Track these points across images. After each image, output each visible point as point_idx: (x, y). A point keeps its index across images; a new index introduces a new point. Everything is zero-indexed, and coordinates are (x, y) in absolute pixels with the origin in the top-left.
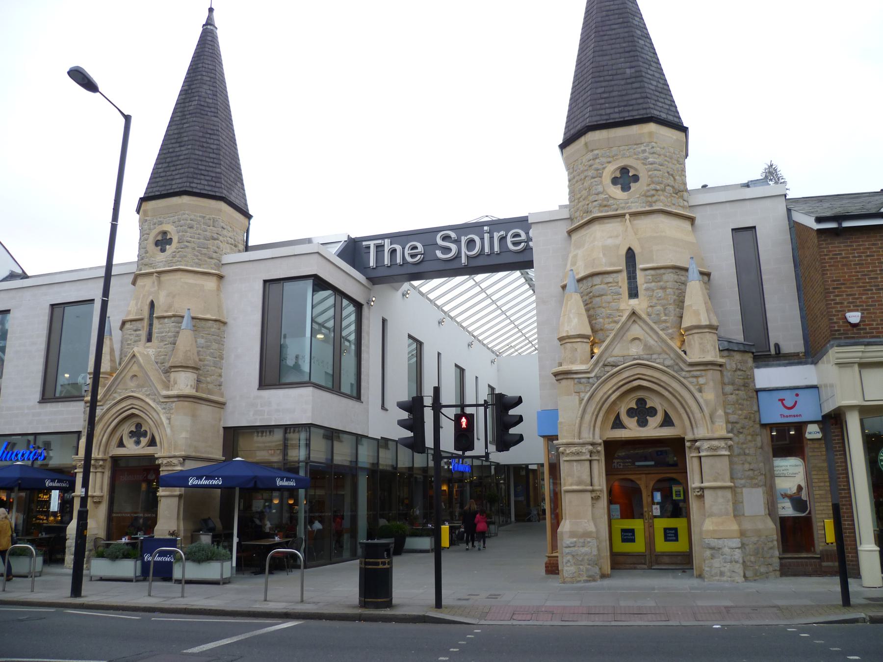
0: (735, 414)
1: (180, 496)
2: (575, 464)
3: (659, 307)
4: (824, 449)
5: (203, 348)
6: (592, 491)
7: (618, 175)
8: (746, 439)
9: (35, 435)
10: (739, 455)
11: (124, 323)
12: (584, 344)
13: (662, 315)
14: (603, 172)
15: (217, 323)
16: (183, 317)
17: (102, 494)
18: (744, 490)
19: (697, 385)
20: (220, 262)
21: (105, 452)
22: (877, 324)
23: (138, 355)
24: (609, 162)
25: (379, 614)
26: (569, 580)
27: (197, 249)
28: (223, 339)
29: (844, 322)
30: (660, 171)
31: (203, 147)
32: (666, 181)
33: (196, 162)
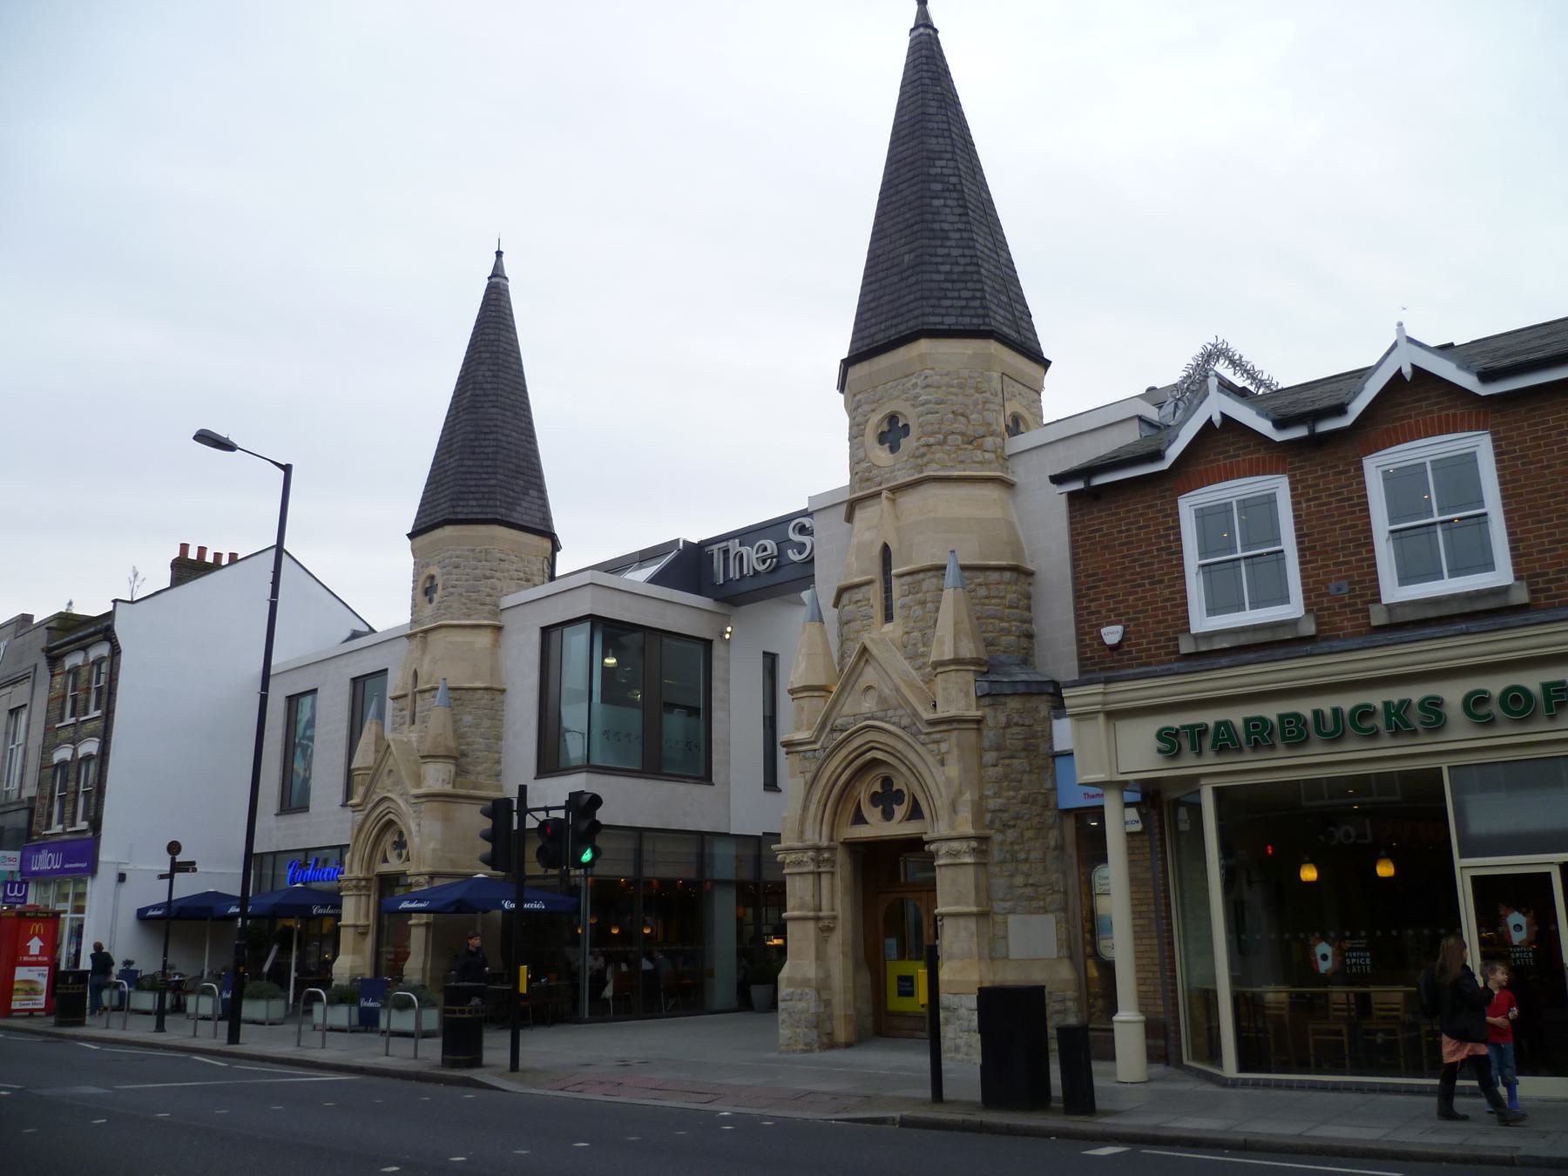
0: (999, 797)
1: (427, 925)
2: (797, 878)
3: (916, 634)
4: (1148, 850)
5: (470, 727)
6: (817, 919)
7: (885, 427)
8: (1022, 836)
9: (307, 851)
10: (1003, 862)
11: (842, 591)
12: (963, 673)
13: (920, 645)
14: (865, 428)
15: (489, 692)
16: (943, 568)
17: (367, 923)
18: (1011, 918)
19: (938, 755)
20: (498, 607)
21: (368, 869)
22: (1149, 643)
23: (870, 646)
24: (873, 411)
25: (454, 1076)
26: (783, 1048)
27: (464, 594)
28: (500, 713)
29: (1098, 644)
30: (937, 413)
31: (474, 453)
32: (946, 427)
33: (464, 477)
